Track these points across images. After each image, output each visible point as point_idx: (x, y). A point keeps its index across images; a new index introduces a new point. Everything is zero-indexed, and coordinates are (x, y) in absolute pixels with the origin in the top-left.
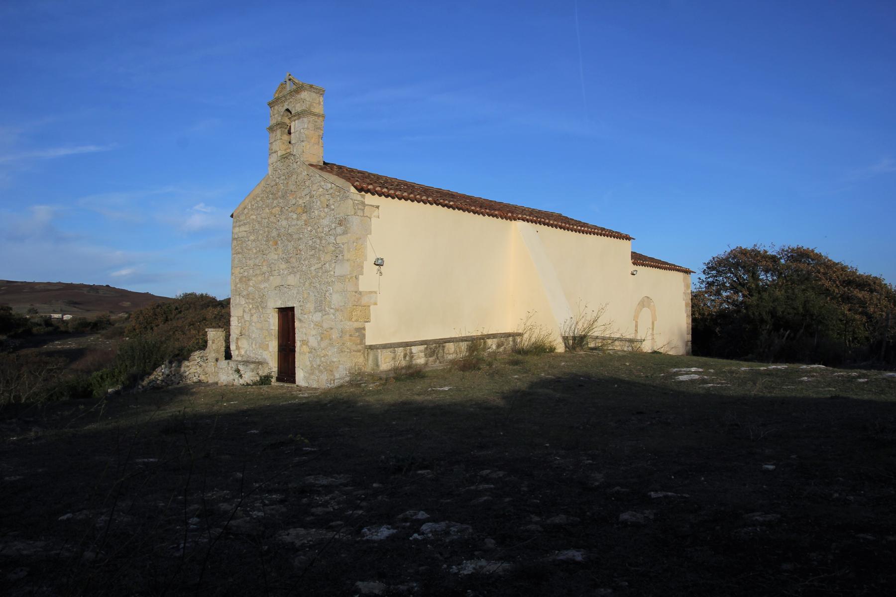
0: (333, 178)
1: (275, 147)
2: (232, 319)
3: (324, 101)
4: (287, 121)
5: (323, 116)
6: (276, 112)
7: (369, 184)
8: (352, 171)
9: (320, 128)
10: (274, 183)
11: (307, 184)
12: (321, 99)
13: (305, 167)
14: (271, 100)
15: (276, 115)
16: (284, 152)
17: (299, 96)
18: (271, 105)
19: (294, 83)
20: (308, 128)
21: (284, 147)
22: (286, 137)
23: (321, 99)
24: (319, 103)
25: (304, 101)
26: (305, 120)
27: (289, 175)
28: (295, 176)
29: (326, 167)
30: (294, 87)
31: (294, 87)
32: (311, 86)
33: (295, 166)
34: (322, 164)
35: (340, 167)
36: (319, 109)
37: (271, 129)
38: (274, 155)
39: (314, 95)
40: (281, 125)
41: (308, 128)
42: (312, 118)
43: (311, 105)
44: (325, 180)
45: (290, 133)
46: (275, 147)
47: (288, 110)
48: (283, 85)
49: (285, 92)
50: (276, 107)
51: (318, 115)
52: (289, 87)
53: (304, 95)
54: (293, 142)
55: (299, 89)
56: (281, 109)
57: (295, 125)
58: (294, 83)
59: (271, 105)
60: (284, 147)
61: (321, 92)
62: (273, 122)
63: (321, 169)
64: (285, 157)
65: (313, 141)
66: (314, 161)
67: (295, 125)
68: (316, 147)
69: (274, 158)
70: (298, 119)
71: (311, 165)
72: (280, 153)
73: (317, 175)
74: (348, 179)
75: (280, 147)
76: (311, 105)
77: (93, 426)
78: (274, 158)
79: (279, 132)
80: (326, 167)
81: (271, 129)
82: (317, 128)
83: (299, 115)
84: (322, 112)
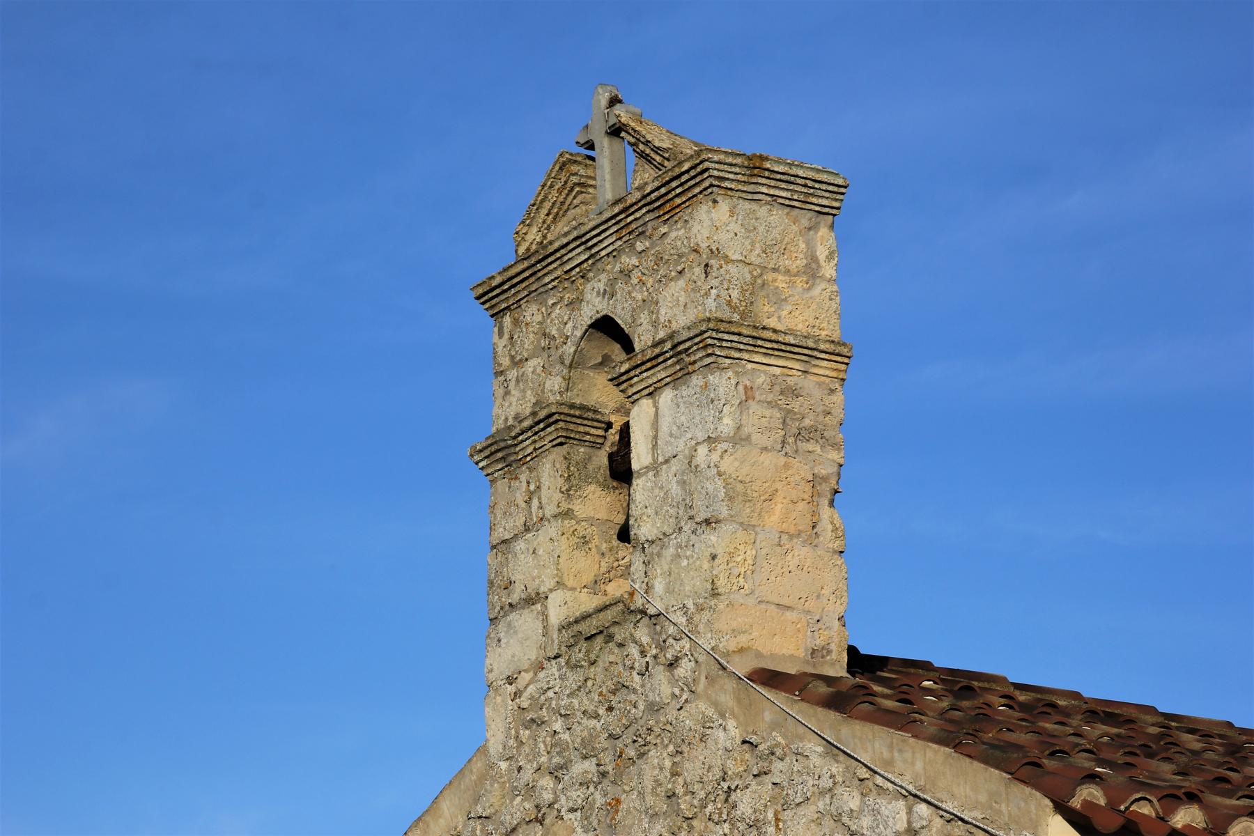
0: (920, 760)
1: (526, 569)
2: (993, 778)
3: (842, 250)
4: (599, 392)
5: (838, 353)
6: (528, 341)
7: (1173, 798)
8: (1040, 704)
9: (813, 434)
10: (520, 808)
11: (745, 804)
12: (824, 240)
13: (727, 693)
14: (494, 260)
15: (533, 365)
16: (589, 602)
17: (676, 234)
18: (498, 297)
19: (646, 153)
20: (739, 439)
21: (586, 566)
22: (596, 503)
23: (824, 240)
24: (811, 271)
25: (710, 260)
26: (723, 383)
27: (626, 749)
28: (659, 759)
29: (871, 685)
30: (647, 176)
31: (647, 176)
32: (756, 166)
33: (662, 685)
34: (837, 667)
35: (962, 684)
36: (807, 311)
37: (503, 453)
38: (526, 621)
39: (774, 221)
40: (561, 423)
41: (739, 439)
42: (763, 372)
43: (755, 287)
44: (867, 778)
45: (621, 471)
46: (526, 569)
47: (606, 327)
48: (572, 170)
49: (585, 214)
50: (532, 313)
51: (802, 350)
52: (613, 177)
53: (713, 222)
54: (644, 530)
55: (678, 186)
56: (564, 318)
57: (658, 423)
58: (646, 153)
59: (498, 297)
60: (586, 566)
61: (816, 197)
62: (512, 406)
63: (839, 700)
64: (590, 634)
65: (775, 517)
66: (786, 648)
67: (658, 423)
68: (801, 552)
69: (522, 641)
70: (678, 380)
71: (770, 678)
72: (558, 609)
73: (813, 745)
74: (1025, 768)
75: (560, 567)
76: (755, 287)
77: (1115, 730)
78: (522, 641)
79: (550, 472)
80: (871, 685)
81: (503, 453)
82: (798, 434)
83: (682, 355)
84: (829, 328)
